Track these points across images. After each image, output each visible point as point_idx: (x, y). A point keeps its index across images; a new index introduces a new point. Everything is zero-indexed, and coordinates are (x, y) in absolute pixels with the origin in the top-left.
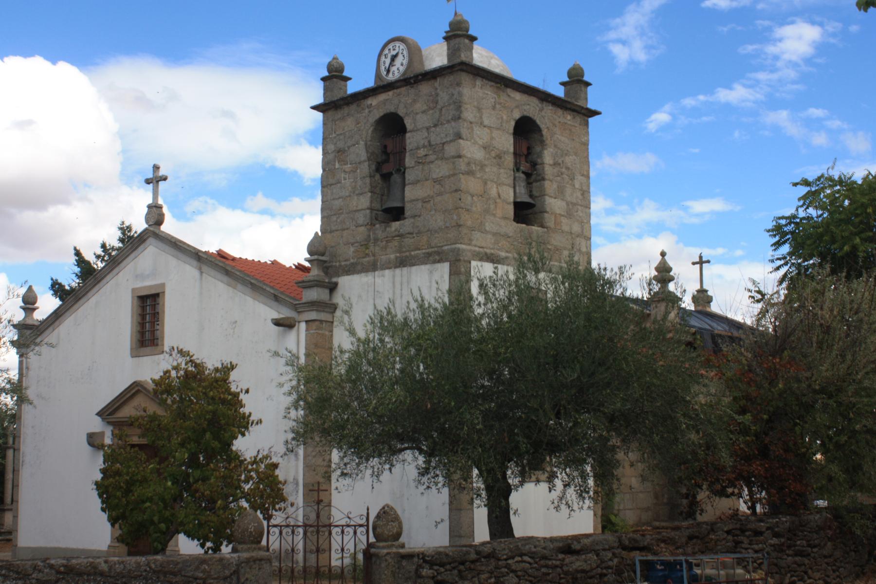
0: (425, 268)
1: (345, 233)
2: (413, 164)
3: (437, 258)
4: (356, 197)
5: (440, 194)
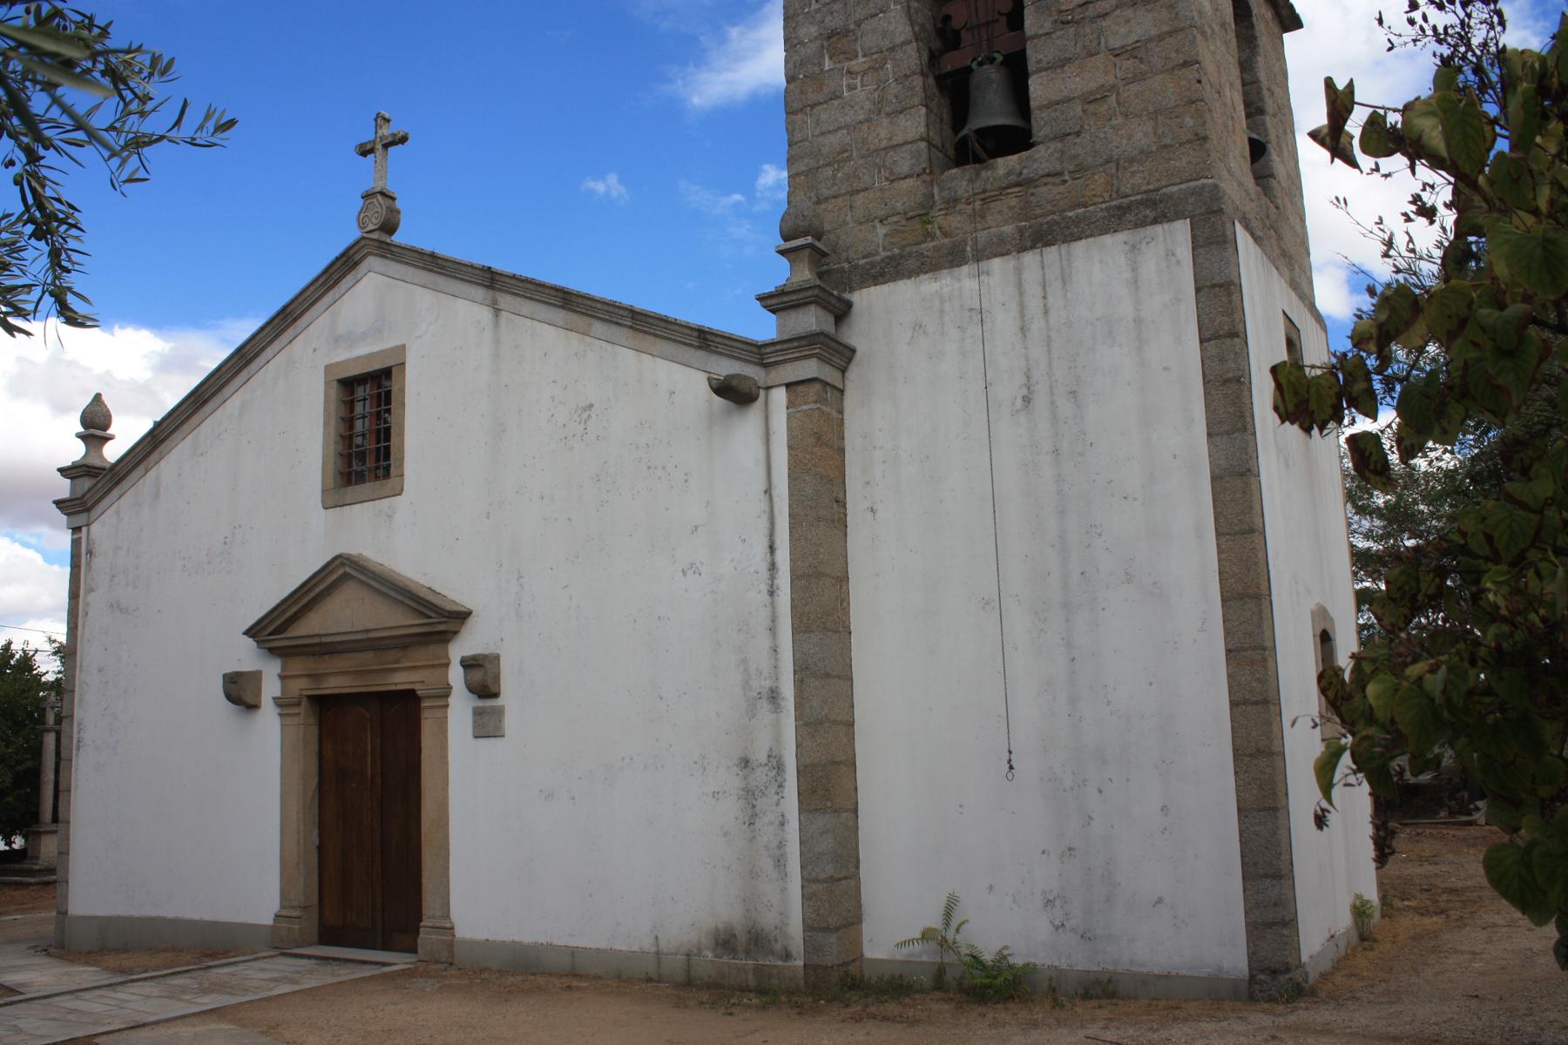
0: (1113, 245)
1: (859, 200)
4: (885, 122)
5: (1139, 77)
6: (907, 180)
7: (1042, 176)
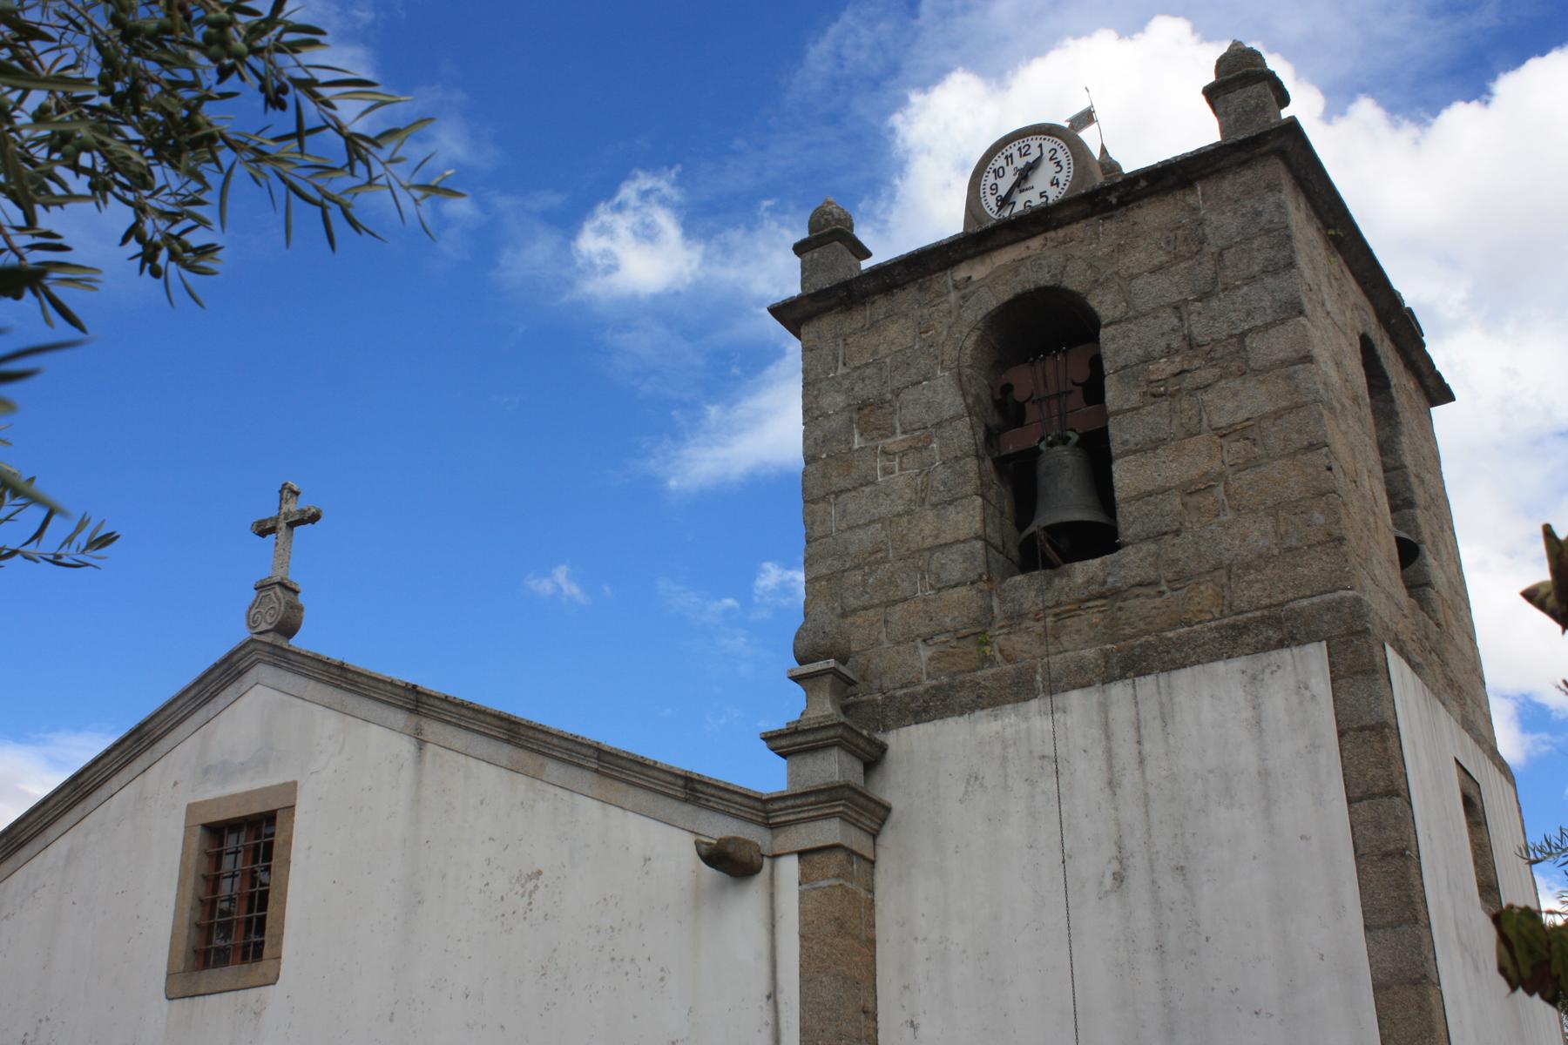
0: (1228, 673)
1: (898, 612)
4: (930, 514)
5: (1251, 463)
6: (958, 589)
7: (1133, 586)
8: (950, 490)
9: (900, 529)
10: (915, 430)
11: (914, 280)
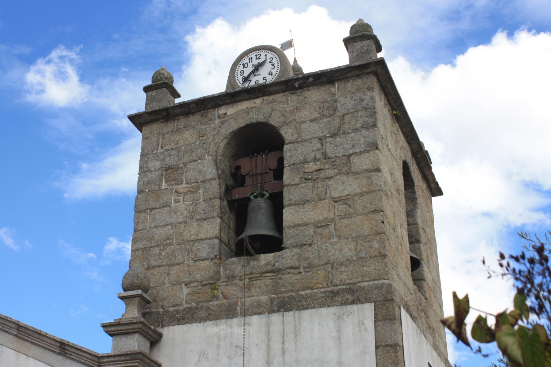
1: (174, 270)
2: (297, 180)
3: (350, 298)
4: (195, 224)
5: (348, 216)
6: (205, 262)
7: (287, 268)
8: (206, 214)
9: (180, 230)
10: (192, 183)
11: (199, 111)
